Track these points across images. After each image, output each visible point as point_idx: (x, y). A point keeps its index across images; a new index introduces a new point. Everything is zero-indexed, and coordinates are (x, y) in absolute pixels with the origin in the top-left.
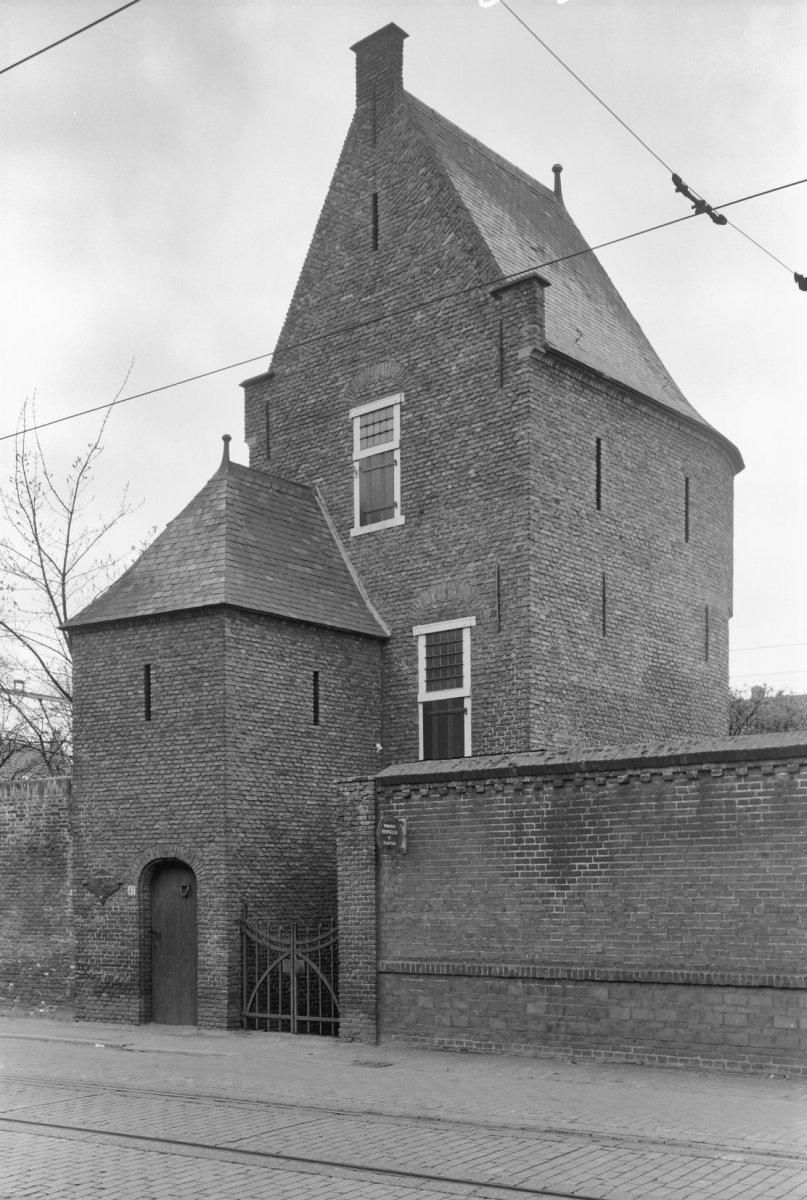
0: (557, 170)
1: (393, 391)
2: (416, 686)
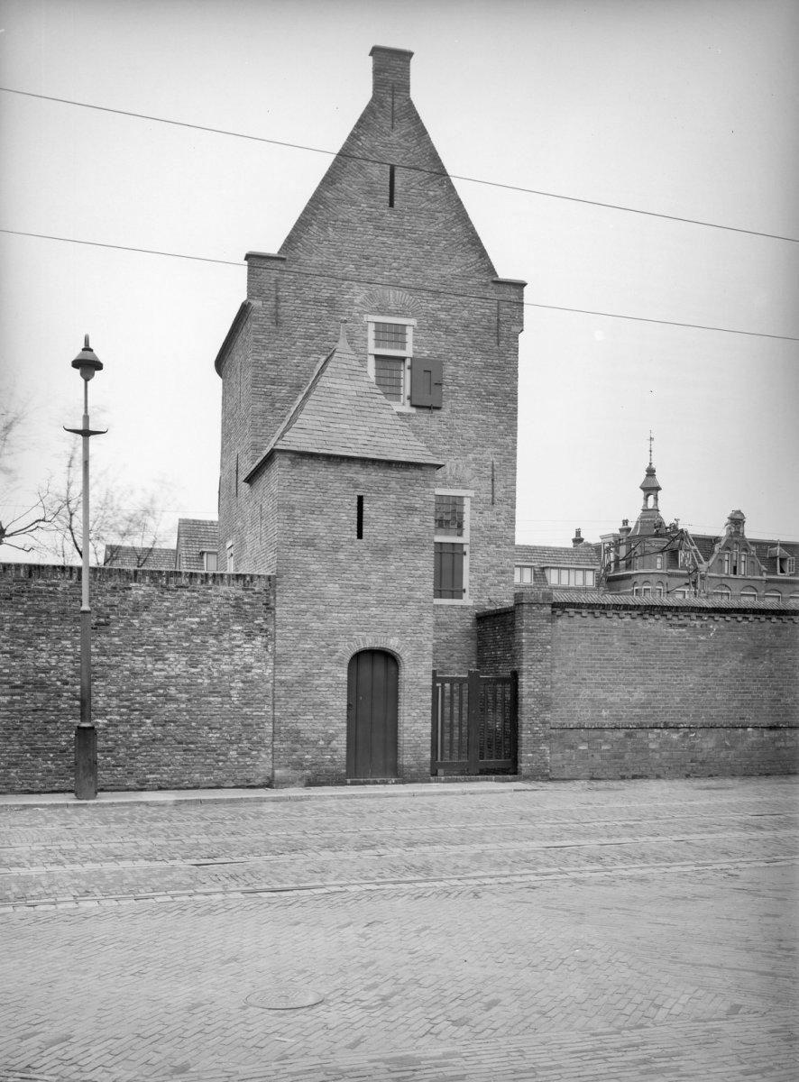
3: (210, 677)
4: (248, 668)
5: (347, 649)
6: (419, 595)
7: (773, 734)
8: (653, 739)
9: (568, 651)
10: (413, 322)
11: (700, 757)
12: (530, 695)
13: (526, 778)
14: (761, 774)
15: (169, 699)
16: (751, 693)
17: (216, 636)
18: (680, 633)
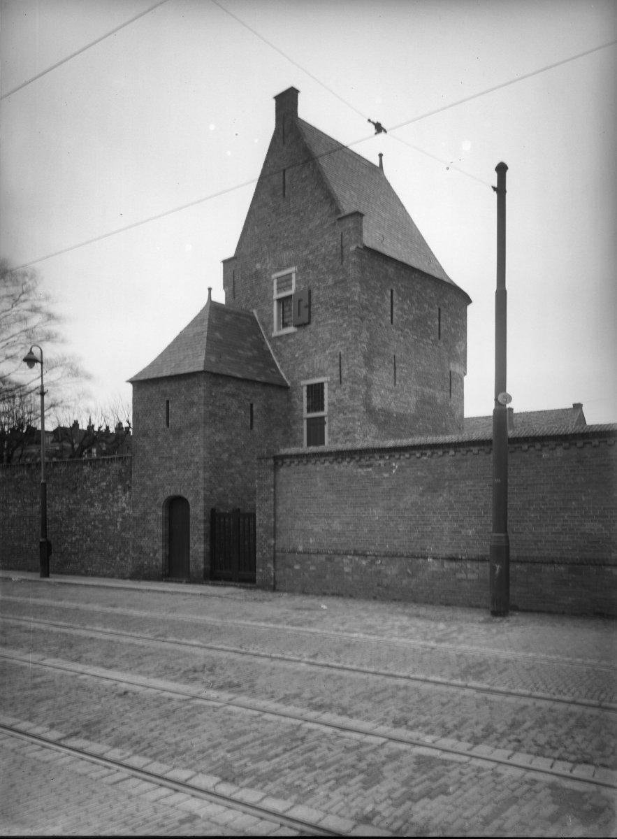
0: (381, 155)
1: (289, 266)
2: (302, 410)
3: (110, 515)
4: (124, 510)
5: (162, 497)
6: (196, 459)
7: (453, 565)
8: (347, 565)
9: (287, 492)
10: (292, 269)
11: (385, 582)
12: (261, 525)
13: (258, 587)
14: (442, 604)
15: (95, 527)
16: (431, 524)
17: (112, 492)
18: (368, 472)
